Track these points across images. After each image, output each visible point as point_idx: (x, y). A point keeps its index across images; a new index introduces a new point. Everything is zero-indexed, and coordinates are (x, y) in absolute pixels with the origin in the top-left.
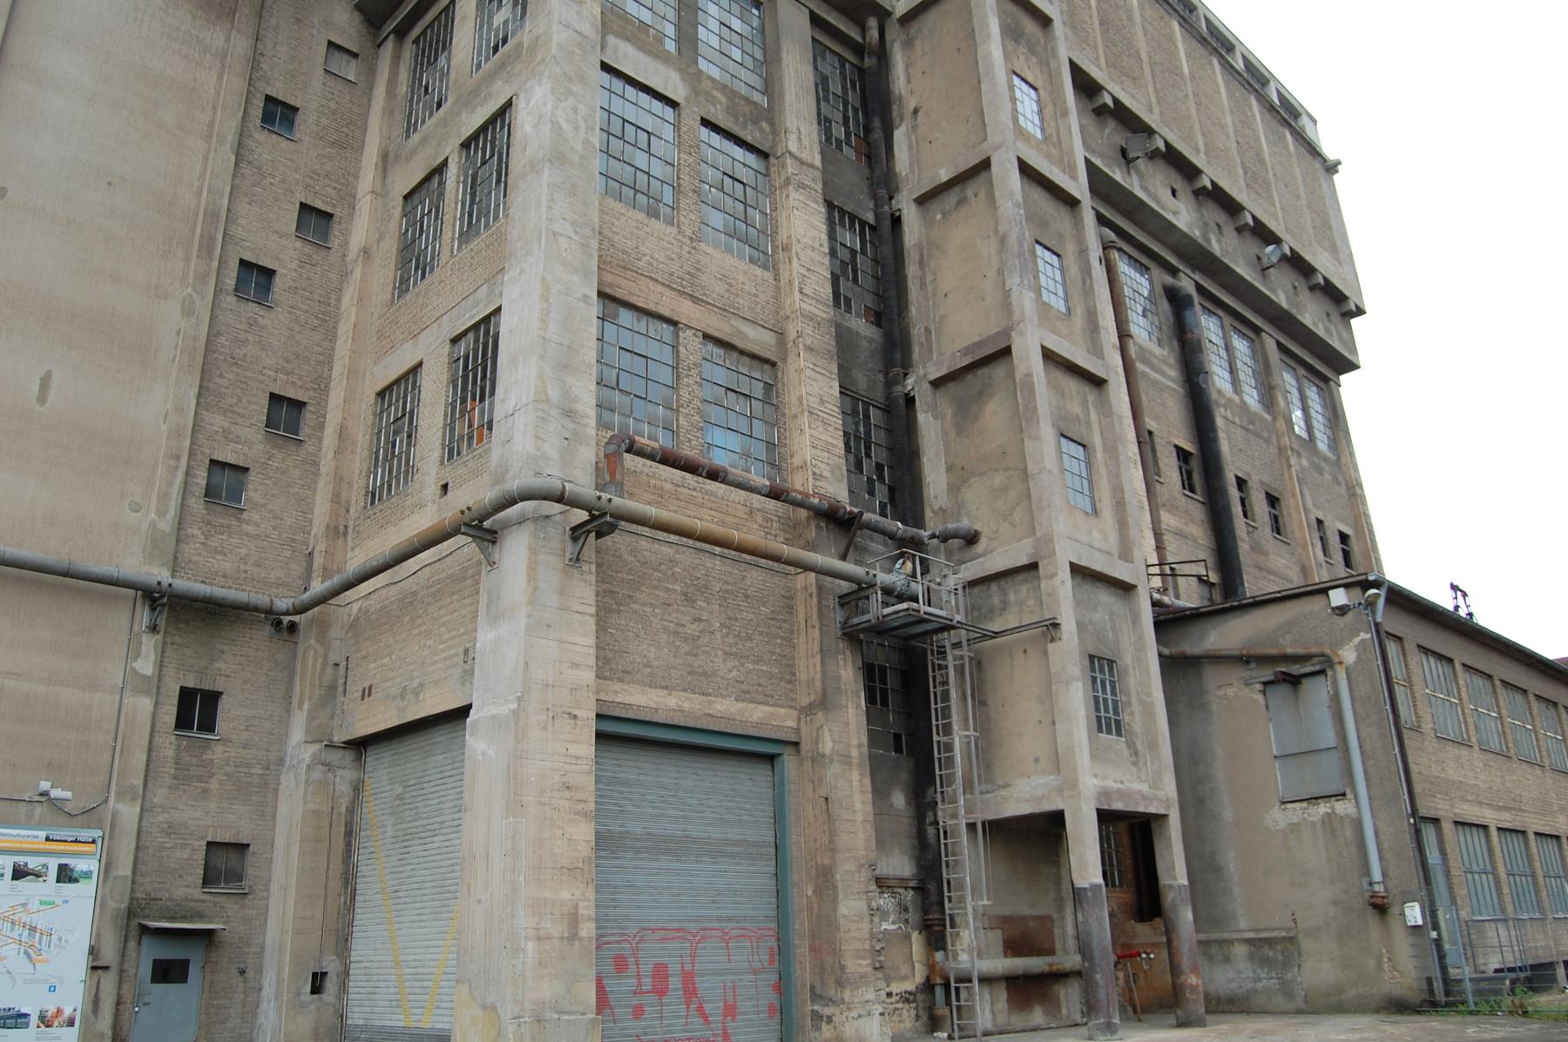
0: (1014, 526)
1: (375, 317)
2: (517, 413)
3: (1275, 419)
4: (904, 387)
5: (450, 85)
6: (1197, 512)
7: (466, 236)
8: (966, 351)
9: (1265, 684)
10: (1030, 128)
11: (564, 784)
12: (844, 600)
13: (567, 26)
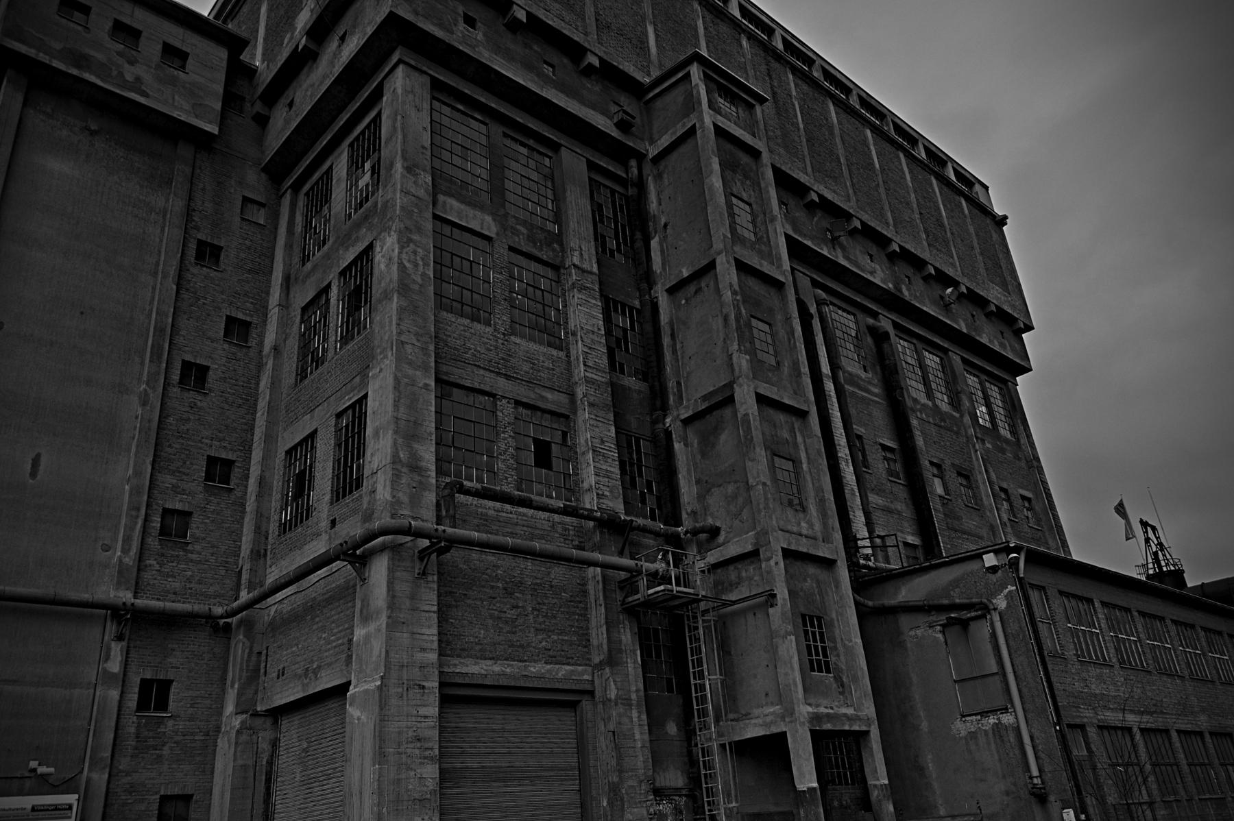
1: (284, 396)
3: (962, 416)
4: (664, 425)
6: (902, 493)
8: (705, 398)
9: (943, 626)
10: (746, 234)
11: (416, 736)
12: (622, 585)
13: (407, 193)
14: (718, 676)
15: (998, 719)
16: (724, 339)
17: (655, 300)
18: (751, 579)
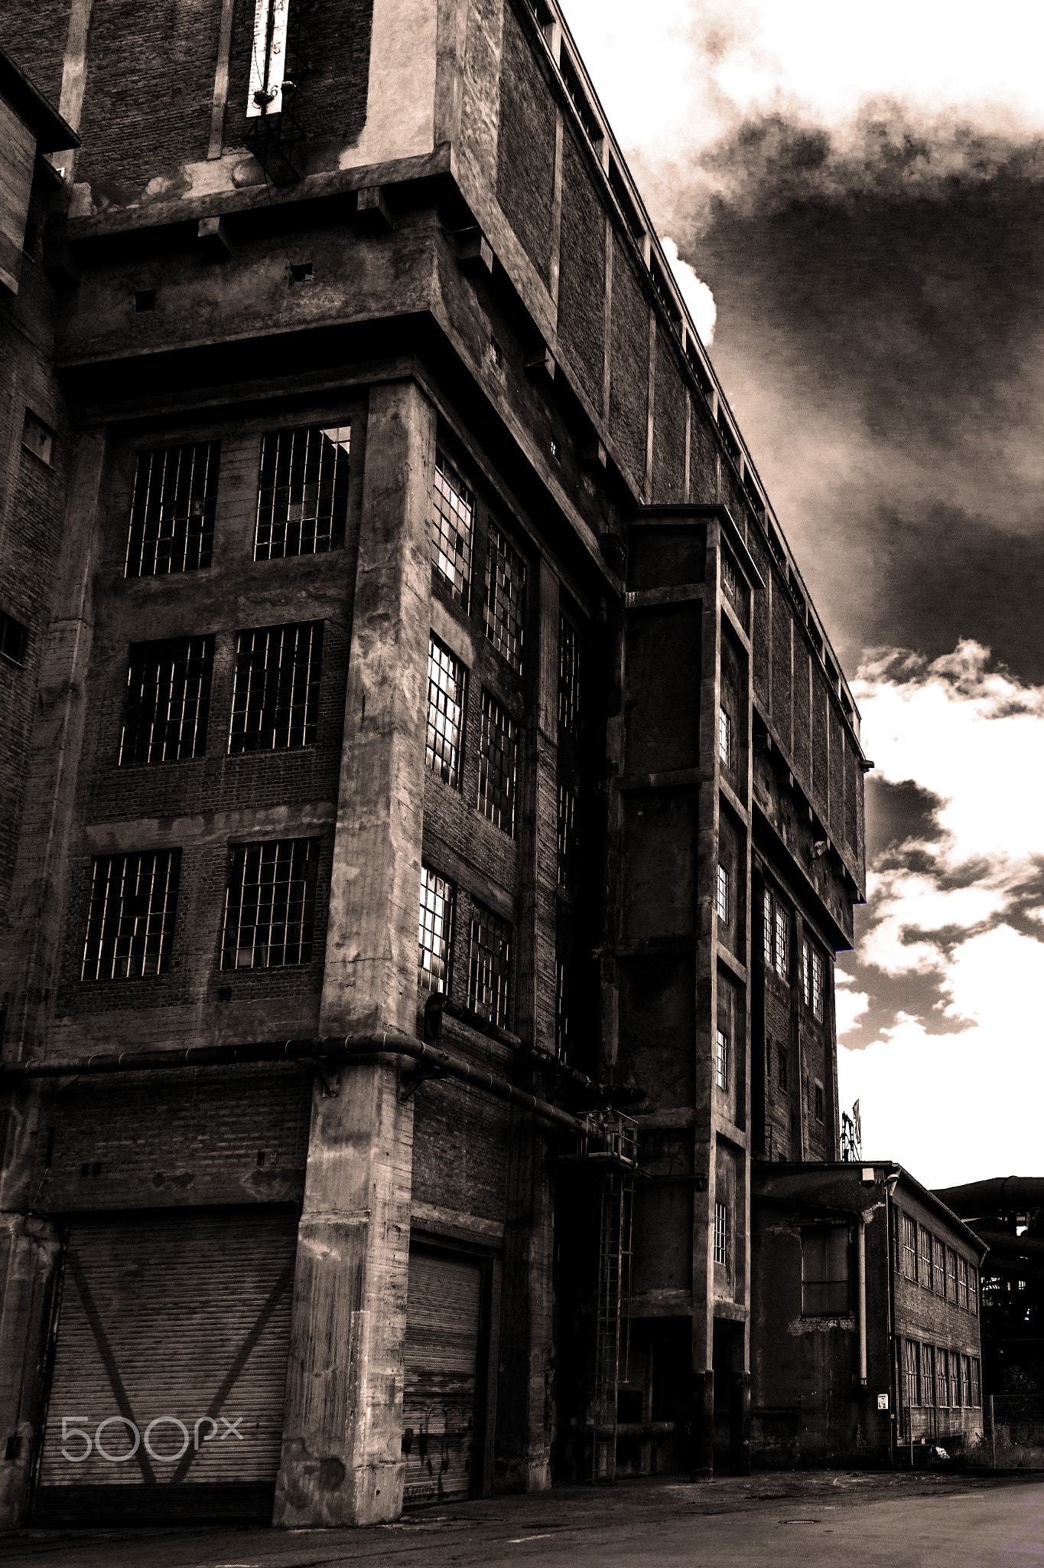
15: (838, 1324)
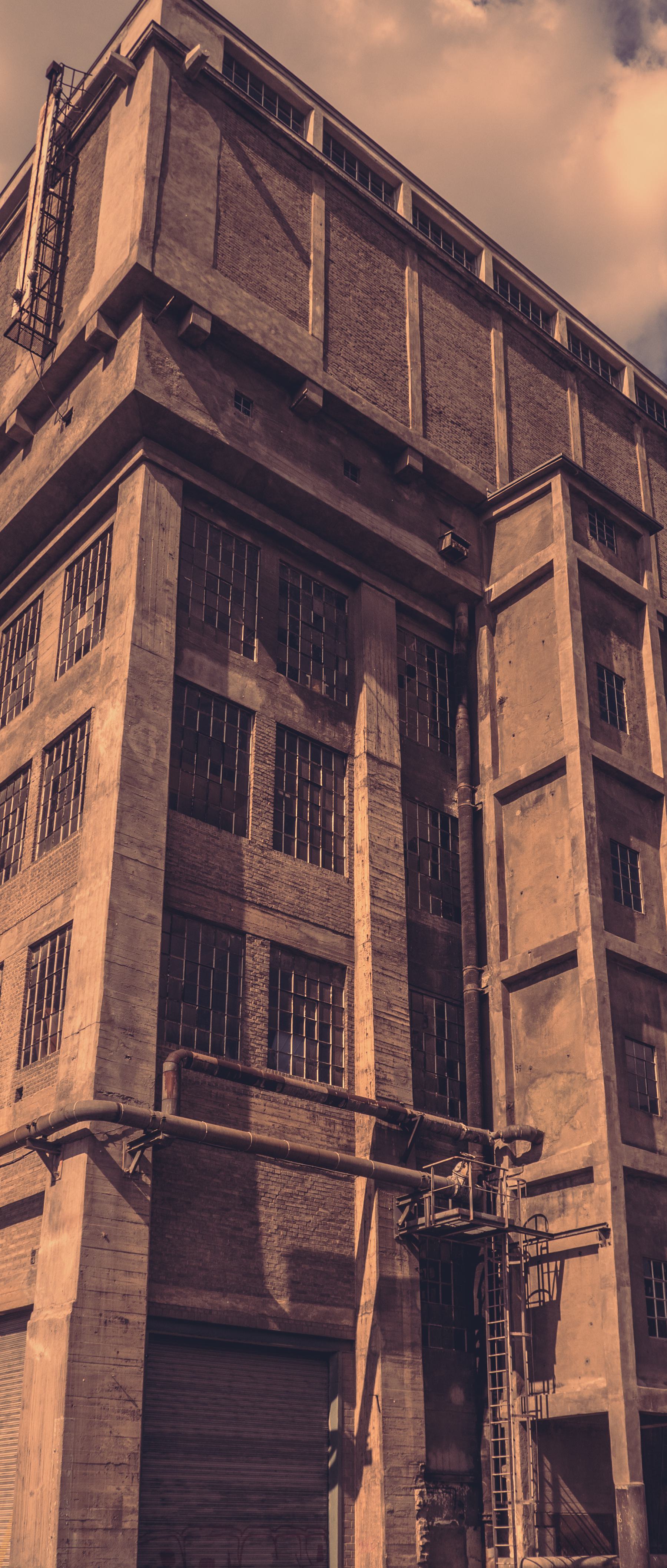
0: (575, 1129)
2: (82, 1032)
4: (479, 985)
5: (36, 686)
7: (48, 840)
8: (537, 952)
14: (524, 1333)
16: (570, 871)
17: (479, 807)
18: (578, 1206)
